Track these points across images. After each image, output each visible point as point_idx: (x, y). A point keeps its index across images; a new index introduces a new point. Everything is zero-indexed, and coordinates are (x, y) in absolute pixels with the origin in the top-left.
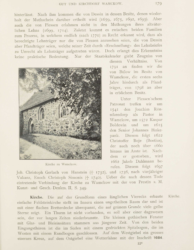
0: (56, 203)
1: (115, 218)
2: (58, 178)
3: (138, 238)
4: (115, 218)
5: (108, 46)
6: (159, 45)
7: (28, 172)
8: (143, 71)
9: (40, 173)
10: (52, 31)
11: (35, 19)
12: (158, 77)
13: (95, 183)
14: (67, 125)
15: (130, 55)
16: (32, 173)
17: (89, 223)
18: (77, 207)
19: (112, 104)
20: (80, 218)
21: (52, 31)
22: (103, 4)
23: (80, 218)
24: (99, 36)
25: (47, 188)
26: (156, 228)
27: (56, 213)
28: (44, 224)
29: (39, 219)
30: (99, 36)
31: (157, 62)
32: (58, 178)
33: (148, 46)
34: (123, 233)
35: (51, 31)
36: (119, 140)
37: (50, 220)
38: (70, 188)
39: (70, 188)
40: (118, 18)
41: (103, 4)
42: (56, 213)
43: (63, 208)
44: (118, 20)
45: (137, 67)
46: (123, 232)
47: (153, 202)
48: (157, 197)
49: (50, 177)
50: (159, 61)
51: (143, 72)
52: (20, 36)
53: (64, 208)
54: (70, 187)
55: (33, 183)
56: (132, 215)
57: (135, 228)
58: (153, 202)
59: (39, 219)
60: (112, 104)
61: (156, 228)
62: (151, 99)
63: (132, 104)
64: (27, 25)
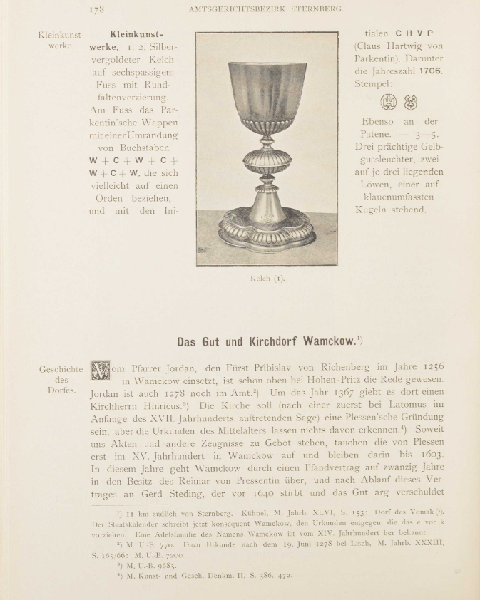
13: (143, 382)
14: (401, 102)
15: (378, 208)
17: (356, 456)
18: (290, 479)
19: (360, 59)
24: (349, 395)
25: (125, 123)
26: (384, 443)
29: (397, 444)
30: (349, 395)
40: (349, 390)
43: (156, 495)
44: (350, 393)
48: (370, 468)
51: (130, 483)
56: (161, 529)
59: (397, 444)
60: (360, 59)
61: (384, 443)
64: (299, 524)
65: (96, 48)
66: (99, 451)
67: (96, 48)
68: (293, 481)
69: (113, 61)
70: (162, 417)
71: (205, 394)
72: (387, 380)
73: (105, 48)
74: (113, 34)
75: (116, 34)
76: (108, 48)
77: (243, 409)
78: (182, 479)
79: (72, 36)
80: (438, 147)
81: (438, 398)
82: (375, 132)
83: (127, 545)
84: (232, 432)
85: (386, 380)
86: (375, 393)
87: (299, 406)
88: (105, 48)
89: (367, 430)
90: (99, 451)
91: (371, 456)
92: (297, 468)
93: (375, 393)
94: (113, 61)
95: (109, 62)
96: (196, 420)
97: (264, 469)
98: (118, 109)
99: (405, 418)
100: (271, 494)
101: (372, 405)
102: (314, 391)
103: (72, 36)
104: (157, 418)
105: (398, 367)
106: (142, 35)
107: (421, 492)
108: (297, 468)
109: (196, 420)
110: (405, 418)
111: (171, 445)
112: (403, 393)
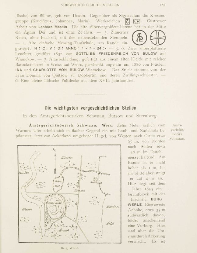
1: (65, 60)
3: (132, 200)
4: (65, 60)
11: (59, 42)
12: (113, 21)
22: (56, 108)
28: (105, 76)
31: (140, 226)
33: (124, 126)
34: (53, 65)
38: (107, 80)
39: (107, 80)
41: (56, 108)
45: (127, 81)
46: (52, 64)
47: (134, 131)
50: (141, 226)
53: (160, 142)
54: (107, 81)
57: (115, 116)
58: (134, 131)
63: (157, 21)
64: (150, 231)
66: (132, 229)
68: (105, 16)
69: (109, 27)
70: (104, 80)
77: (94, 66)
80: (126, 131)
82: (127, 135)
84: (141, 173)
86: (53, 131)
87: (60, 16)
89: (104, 21)
90: (132, 229)
91: (154, 215)
93: (53, 131)
94: (109, 27)
96: (144, 226)
100: (134, 152)
101: (161, 131)
102: (114, 80)
104: (102, 80)
105: (114, 81)
107: (120, 80)
109: (144, 226)
111: (112, 43)
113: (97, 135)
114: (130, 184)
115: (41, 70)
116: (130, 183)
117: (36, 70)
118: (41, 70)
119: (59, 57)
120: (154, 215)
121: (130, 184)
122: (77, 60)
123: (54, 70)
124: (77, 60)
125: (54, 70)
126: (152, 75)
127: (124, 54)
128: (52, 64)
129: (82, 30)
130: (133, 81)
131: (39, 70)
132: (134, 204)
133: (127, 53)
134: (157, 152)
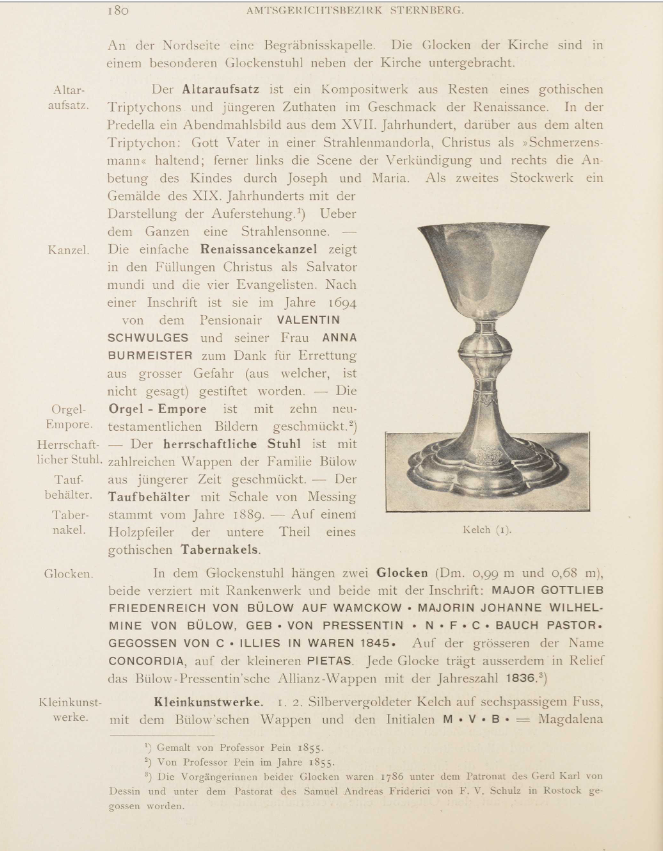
0: (151, 109)
2: (212, 126)
5: (303, 357)
6: (149, 530)
7: (56, 409)
8: (140, 676)
9: (316, 179)
10: (495, 574)
16: (463, 144)
20: (130, 126)
21: (495, 574)
23: (130, 126)
27: (287, 531)
29: (350, 704)
32: (212, 126)
34: (267, 722)
35: (491, 574)
36: (257, 569)
37: (359, 709)
42: (287, 531)
45: (403, 144)
49: (230, 267)
51: (140, 680)
52: (218, 357)
54: (368, 126)
55: (278, 197)
62: (242, 680)
65: (232, 704)
67: (232, 704)
69: (374, 703)
71: (453, 592)
72: (578, 662)
73: (244, 704)
74: (157, 702)
75: (163, 701)
76: (248, 704)
78: (231, 588)
79: (86, 703)
81: (595, 99)
83: (142, 626)
85: (578, 661)
88: (244, 704)
92: (222, 357)
95: (369, 705)
97: (531, 46)
98: (581, 700)
99: (112, 198)
103: (86, 703)
105: (387, 125)
106: (199, 704)
108: (222, 357)
110: (112, 198)
112: (448, 644)
113: (114, 529)
114: (114, 534)
115: (327, 643)
116: (114, 529)
117: (529, 625)
118: (327, 643)
119: (204, 472)
120: (249, 179)
121: (114, 534)
122: (172, 216)
123: (174, 355)
124: (172, 216)
125: (174, 355)
126: (484, 178)
127: (526, 625)
128: (186, 459)
129: (208, 366)
130: (452, 126)
131: (506, 609)
132: (183, 354)
133: (534, 623)
134: (262, 179)
